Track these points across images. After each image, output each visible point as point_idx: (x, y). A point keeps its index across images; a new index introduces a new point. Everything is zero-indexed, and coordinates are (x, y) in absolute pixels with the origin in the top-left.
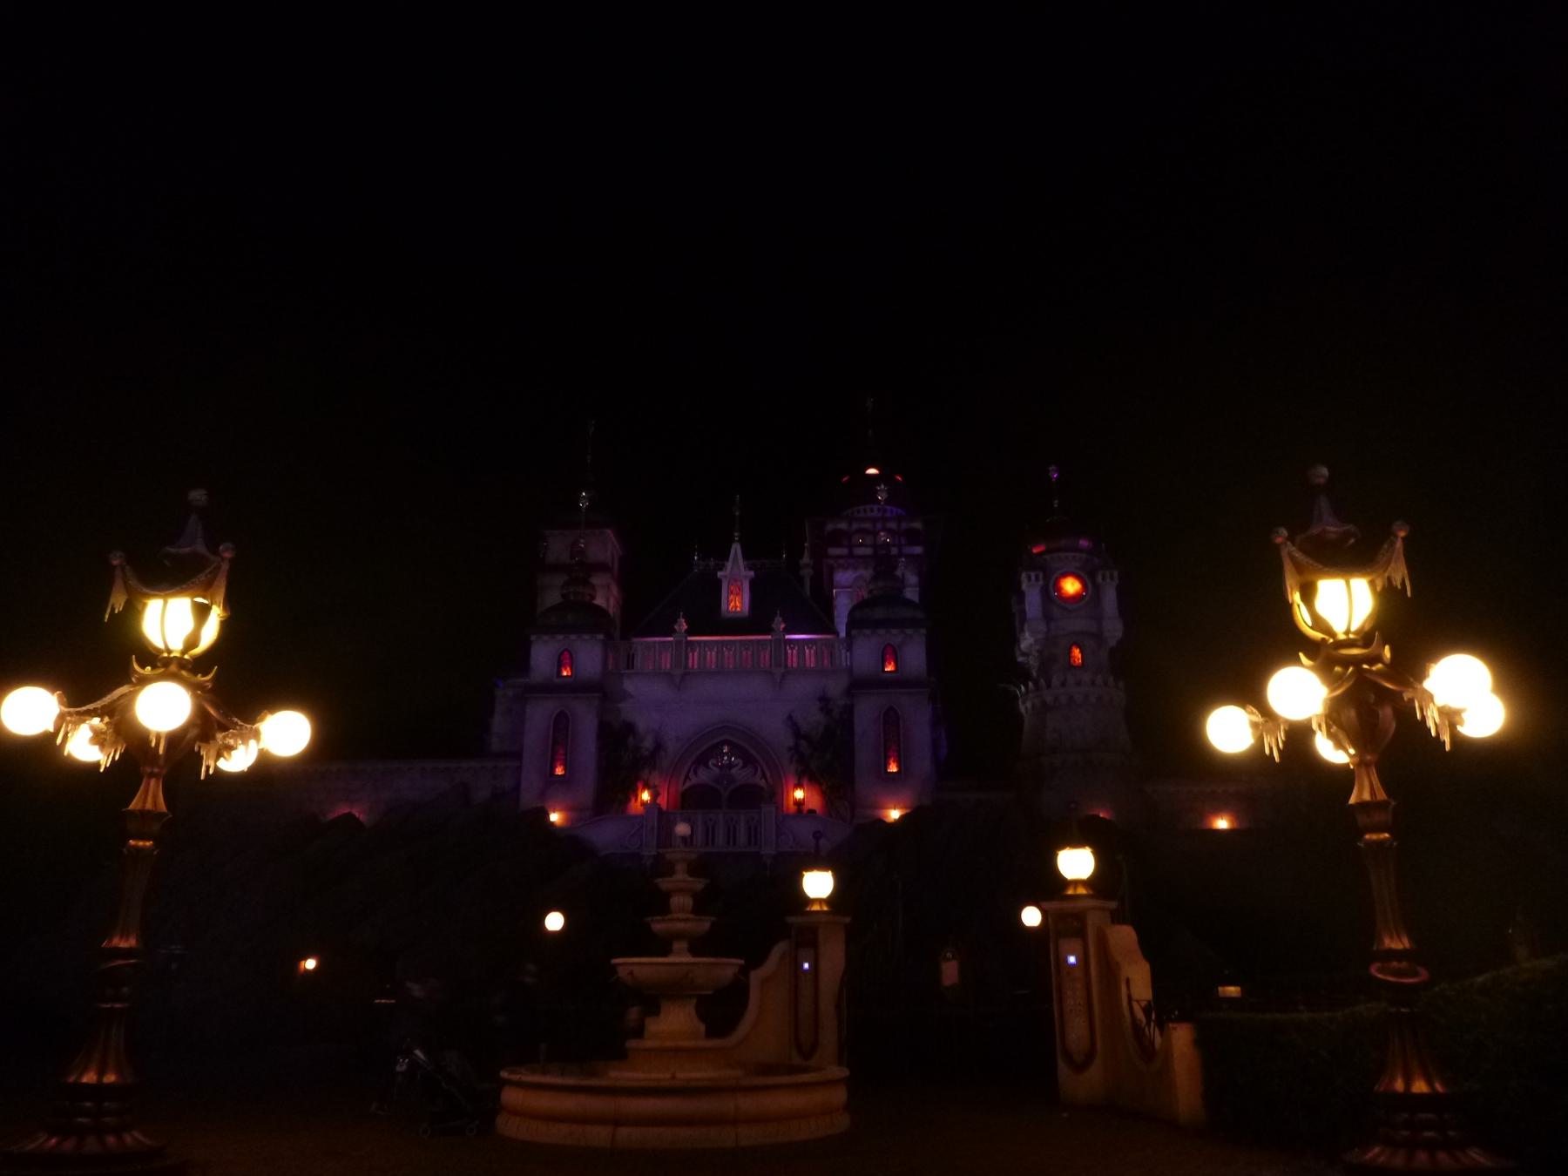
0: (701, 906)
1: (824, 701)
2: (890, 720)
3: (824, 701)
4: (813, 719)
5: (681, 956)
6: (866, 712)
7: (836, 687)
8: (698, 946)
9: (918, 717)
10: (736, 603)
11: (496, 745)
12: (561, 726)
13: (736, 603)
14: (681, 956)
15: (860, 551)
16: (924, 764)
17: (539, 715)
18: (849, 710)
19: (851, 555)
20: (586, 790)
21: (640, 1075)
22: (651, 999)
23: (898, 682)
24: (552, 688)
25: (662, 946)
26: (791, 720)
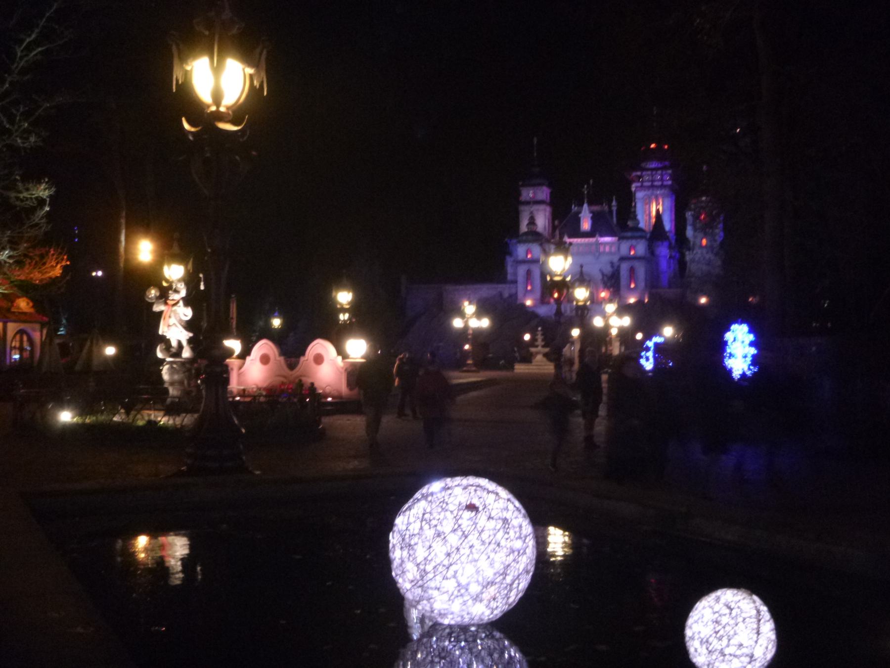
0: (543, 340)
1: (612, 264)
2: (632, 270)
3: (612, 264)
4: (608, 270)
5: (540, 348)
6: (625, 267)
7: (615, 259)
8: (543, 346)
9: (641, 270)
10: (586, 225)
11: (509, 277)
12: (529, 273)
13: (586, 225)
14: (540, 348)
15: (646, 184)
16: (642, 284)
17: (522, 270)
18: (619, 267)
19: (642, 186)
20: (538, 294)
21: (235, 316)
22: (537, 353)
23: (635, 258)
24: (525, 262)
25: (537, 346)
26: (601, 270)
